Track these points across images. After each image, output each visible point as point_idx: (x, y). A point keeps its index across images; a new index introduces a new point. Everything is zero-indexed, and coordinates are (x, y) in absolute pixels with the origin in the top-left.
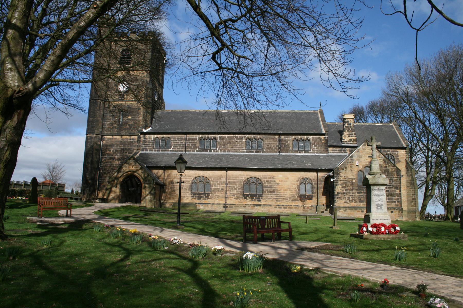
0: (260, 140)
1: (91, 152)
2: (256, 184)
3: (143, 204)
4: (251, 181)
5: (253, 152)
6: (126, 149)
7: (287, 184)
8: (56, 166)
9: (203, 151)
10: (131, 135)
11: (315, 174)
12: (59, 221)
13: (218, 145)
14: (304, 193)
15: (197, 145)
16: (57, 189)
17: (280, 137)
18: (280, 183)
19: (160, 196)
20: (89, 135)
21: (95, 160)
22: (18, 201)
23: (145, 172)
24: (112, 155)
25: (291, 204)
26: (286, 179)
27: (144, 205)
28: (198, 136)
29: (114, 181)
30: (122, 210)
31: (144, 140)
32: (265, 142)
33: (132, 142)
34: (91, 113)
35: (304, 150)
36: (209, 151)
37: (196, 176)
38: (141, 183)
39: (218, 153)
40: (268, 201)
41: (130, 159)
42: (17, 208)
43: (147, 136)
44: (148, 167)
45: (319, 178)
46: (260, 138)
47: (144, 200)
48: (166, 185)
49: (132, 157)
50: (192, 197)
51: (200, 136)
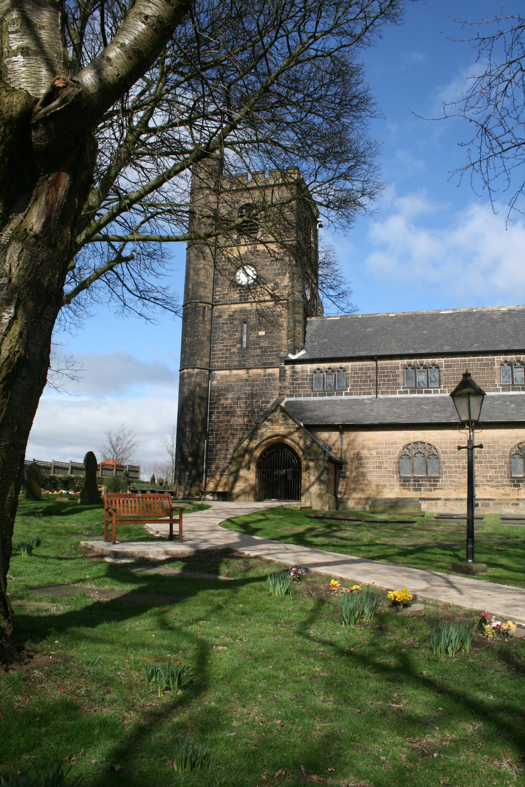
8: (122, 436)
9: (412, 392)
10: (265, 366)
12: (154, 551)
13: (443, 378)
15: (400, 380)
16: (127, 475)
19: (336, 486)
20: (185, 371)
22: (59, 500)
27: (308, 504)
28: (400, 362)
29: (243, 456)
30: (271, 516)
31: (292, 376)
33: (269, 380)
34: (189, 329)
36: (426, 392)
37: (407, 442)
38: (298, 458)
39: (443, 395)
42: (59, 513)
43: (298, 367)
44: (308, 427)
47: (307, 494)
48: (346, 463)
49: (277, 405)
51: (405, 362)
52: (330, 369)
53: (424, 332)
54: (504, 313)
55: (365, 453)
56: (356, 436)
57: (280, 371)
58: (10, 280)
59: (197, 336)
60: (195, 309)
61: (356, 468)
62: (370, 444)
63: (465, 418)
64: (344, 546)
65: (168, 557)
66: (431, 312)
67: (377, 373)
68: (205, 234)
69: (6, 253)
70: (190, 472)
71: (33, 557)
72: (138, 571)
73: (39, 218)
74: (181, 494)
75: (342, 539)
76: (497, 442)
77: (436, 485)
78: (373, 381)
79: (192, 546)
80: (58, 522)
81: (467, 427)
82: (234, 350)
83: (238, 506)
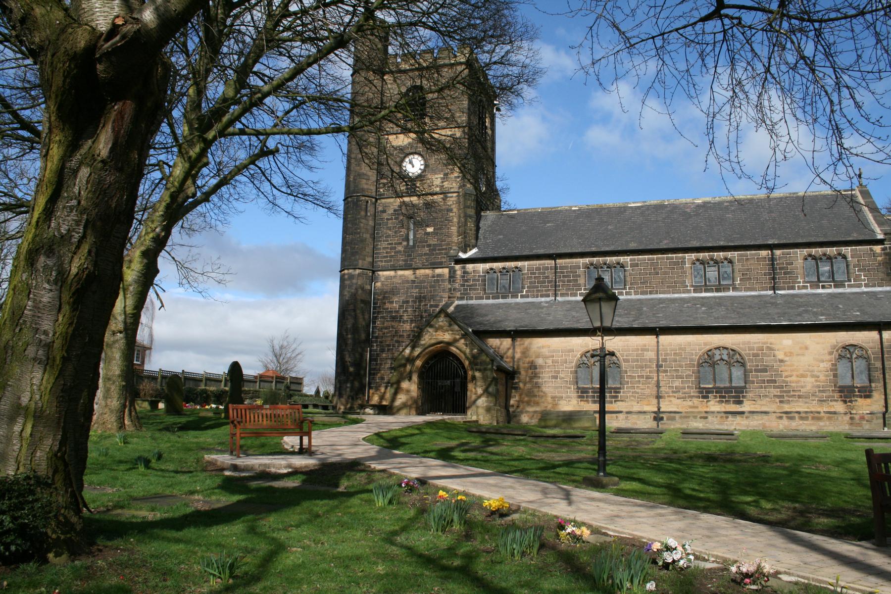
0: (726, 262)
1: (351, 307)
2: (728, 363)
3: (471, 416)
4: (717, 357)
5: (711, 291)
6: (424, 297)
7: (804, 361)
8: (285, 344)
10: (434, 266)
11: (874, 334)
12: (279, 464)
13: (628, 279)
14: (847, 382)
16: (288, 388)
17: (772, 254)
18: (787, 359)
19: (508, 398)
20: (346, 271)
21: (362, 322)
22: (203, 414)
23: (472, 345)
24: (397, 312)
25: (819, 410)
26: (801, 348)
27: (474, 418)
28: (581, 261)
29: (405, 366)
30: (428, 431)
31: (463, 277)
32: (738, 266)
34: (349, 225)
35: (834, 281)
38: (463, 367)
39: (629, 297)
40: (759, 402)
41: (437, 316)
43: (470, 267)
44: (477, 333)
45: (885, 344)
46: (726, 259)
47: (474, 408)
48: (520, 373)
49: (443, 311)
50: (579, 397)
51: (587, 260)
52: (504, 268)
53: (610, 227)
54: (699, 206)
55: (540, 361)
56: (530, 344)
57: (450, 272)
58: (79, 202)
59: (359, 233)
60: (356, 204)
61: (531, 378)
62: (545, 351)
63: (597, 324)
64: (467, 460)
65: (290, 470)
66: (619, 205)
67: (556, 273)
68: (363, 123)
69: (76, 177)
70: (352, 383)
71: (149, 471)
72: (254, 484)
73: (106, 144)
74: (342, 407)
75: (492, 453)
76: (684, 349)
77: (617, 397)
78: (551, 282)
79: (320, 459)
80: (191, 437)
81: (599, 333)
82: (400, 248)
83: (394, 420)
